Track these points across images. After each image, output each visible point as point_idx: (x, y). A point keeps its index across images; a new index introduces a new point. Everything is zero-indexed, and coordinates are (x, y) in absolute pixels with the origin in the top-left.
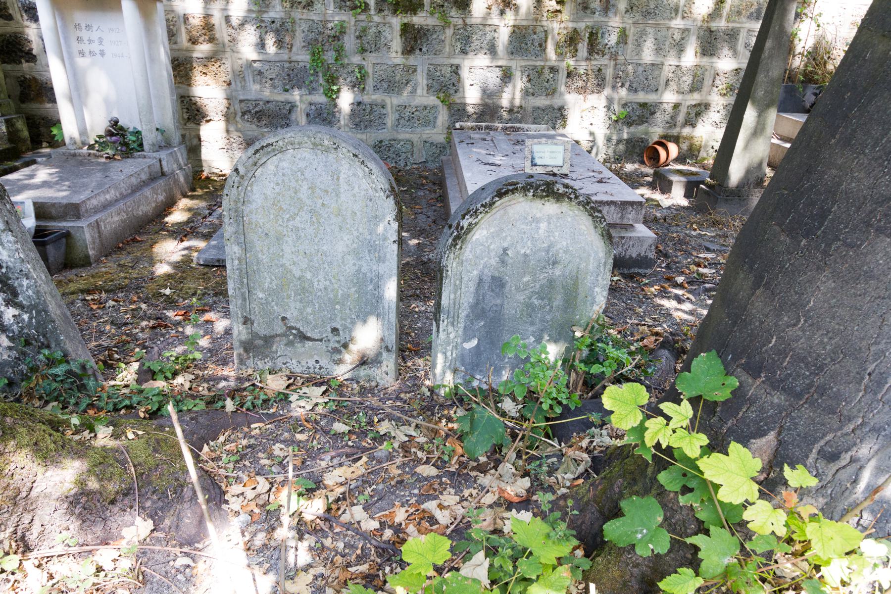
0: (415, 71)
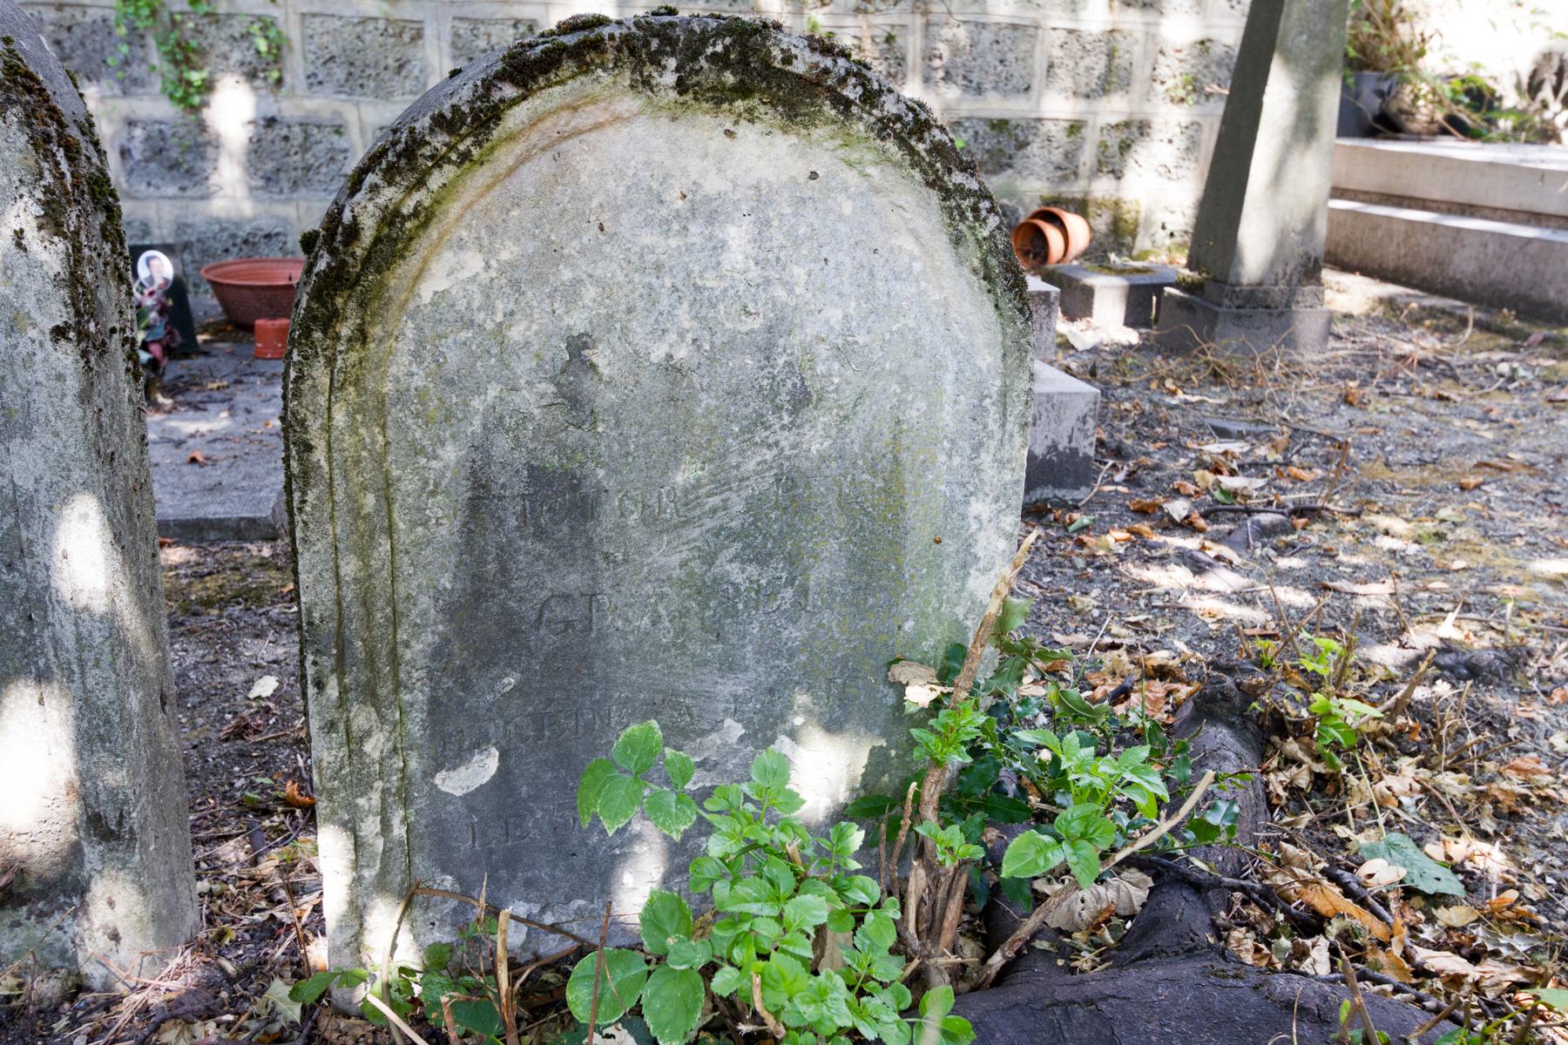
0: (418, 36)
